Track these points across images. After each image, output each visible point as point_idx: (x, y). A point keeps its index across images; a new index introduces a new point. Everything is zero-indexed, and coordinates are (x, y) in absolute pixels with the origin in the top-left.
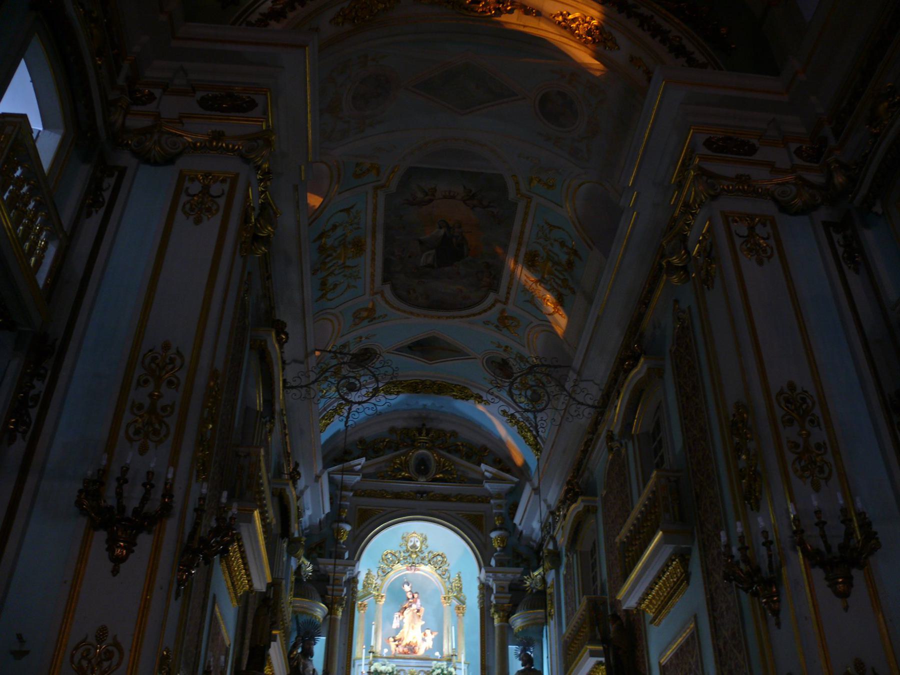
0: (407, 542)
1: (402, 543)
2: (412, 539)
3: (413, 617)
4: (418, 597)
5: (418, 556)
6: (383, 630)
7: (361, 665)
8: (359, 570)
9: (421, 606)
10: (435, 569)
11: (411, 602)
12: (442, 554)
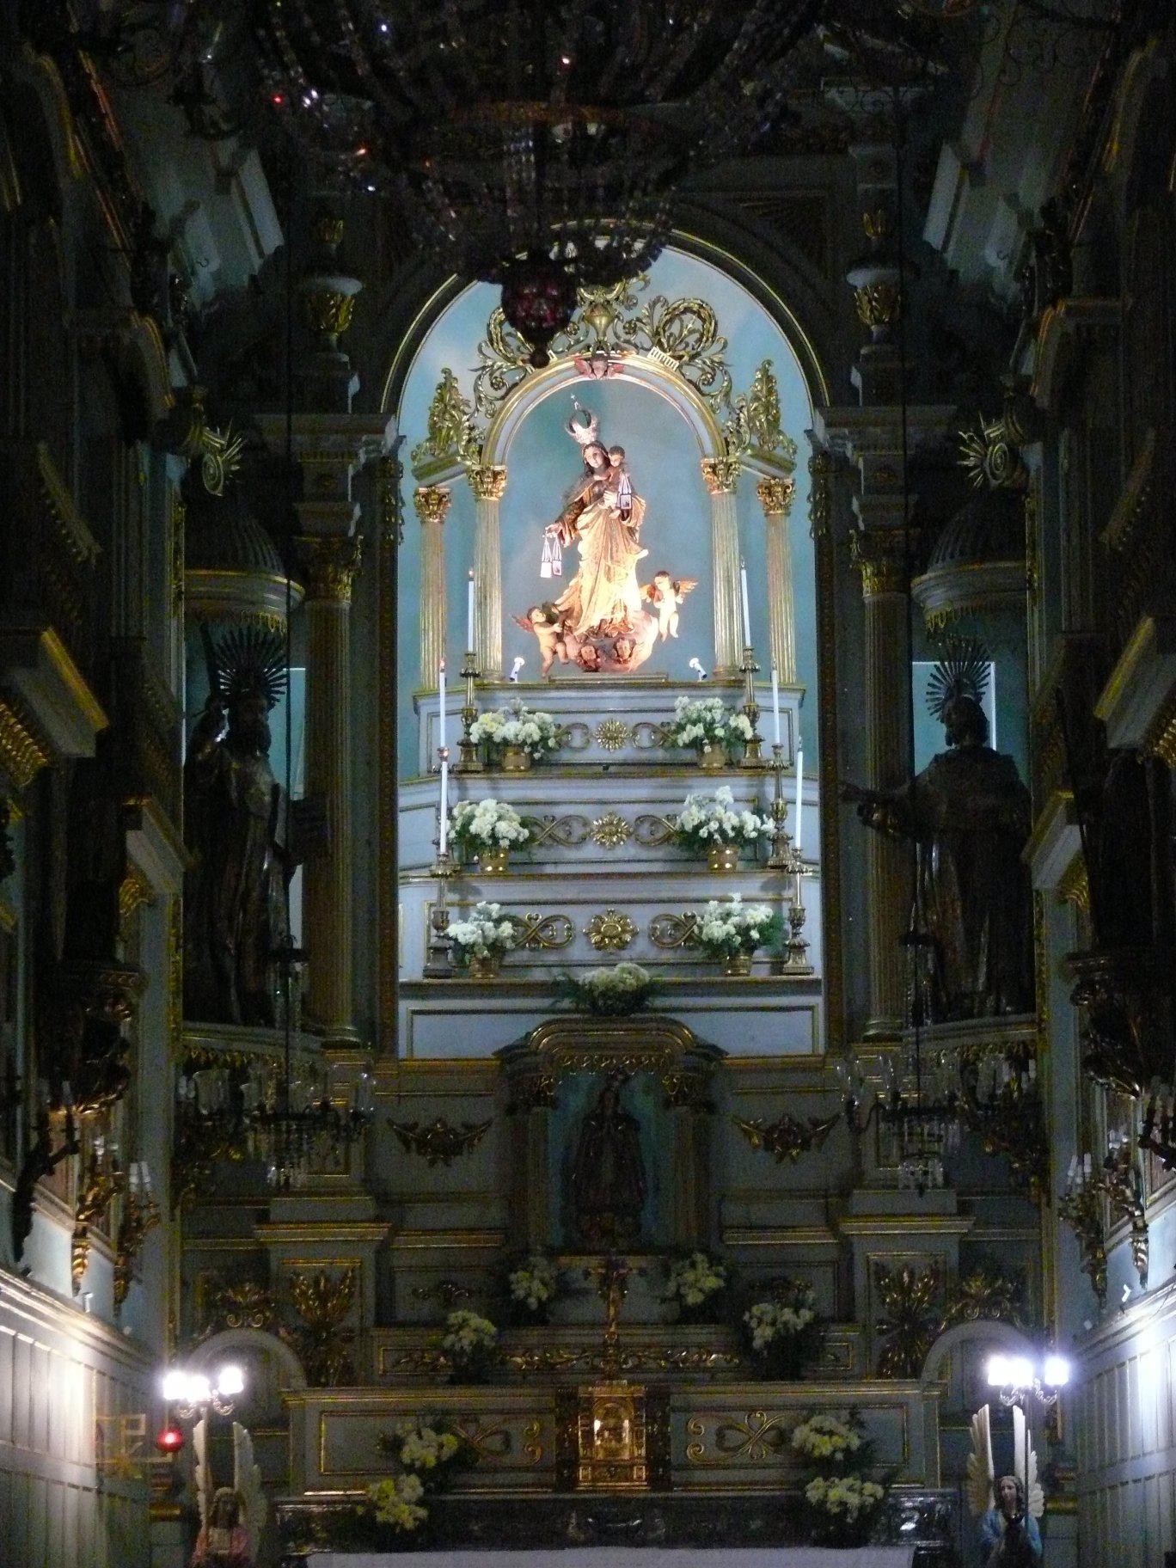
3: (610, 537)
4: (621, 464)
7: (437, 715)
8: (401, 434)
9: (633, 494)
10: (677, 363)
11: (599, 483)
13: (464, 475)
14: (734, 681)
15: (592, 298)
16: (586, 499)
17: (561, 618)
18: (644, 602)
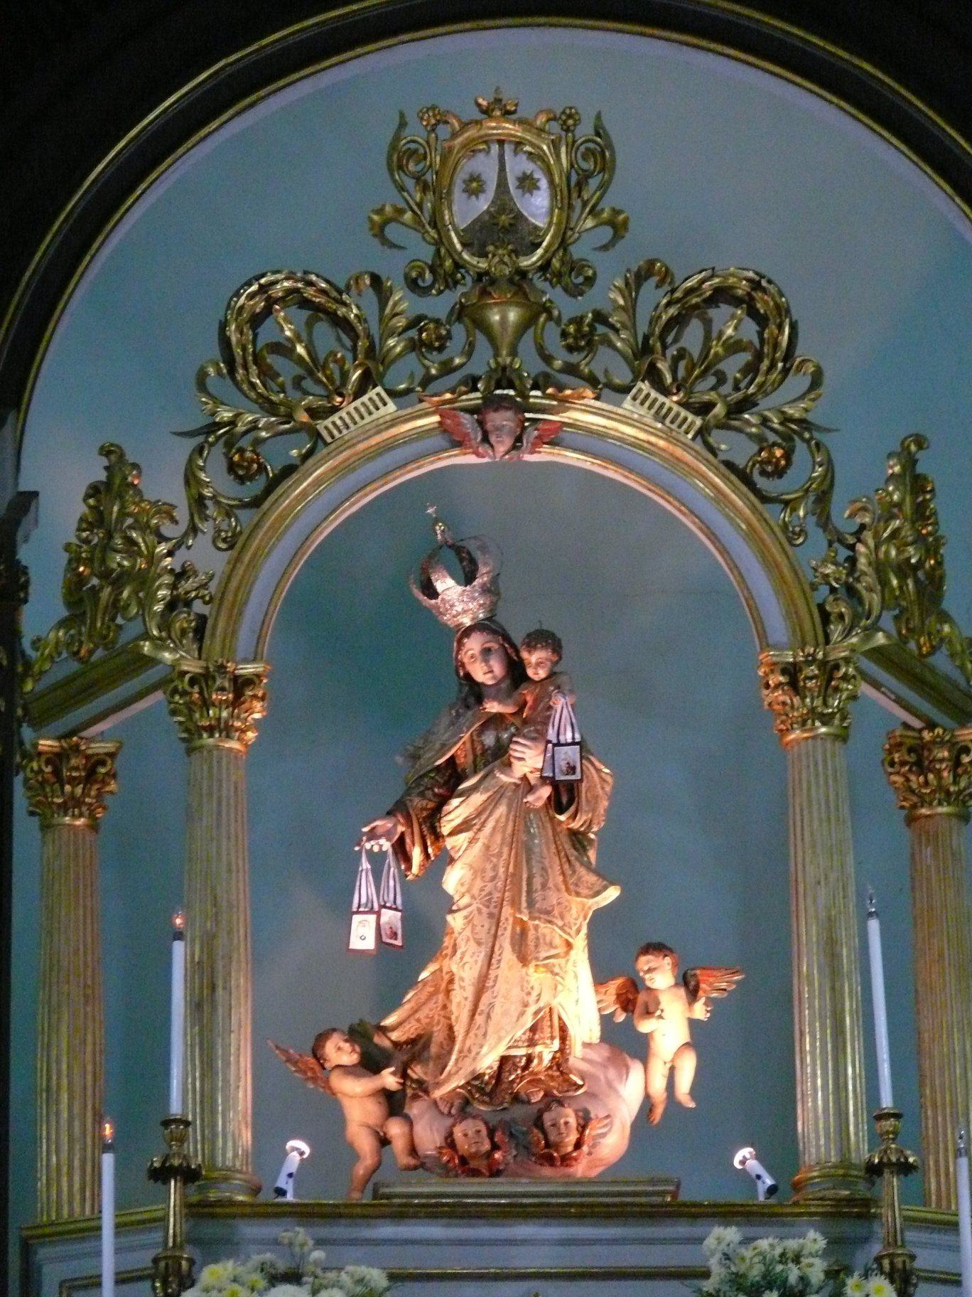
0: (442, 195)
1: (391, 198)
2: (486, 166)
3: (522, 848)
4: (551, 675)
5: (536, 312)
6: (258, 961)
8: (24, 486)
11: (496, 721)
12: (756, 285)
13: (159, 696)
14: (850, 1201)
15: (483, 265)
16: (464, 761)
17: (403, 1057)
18: (606, 1021)
